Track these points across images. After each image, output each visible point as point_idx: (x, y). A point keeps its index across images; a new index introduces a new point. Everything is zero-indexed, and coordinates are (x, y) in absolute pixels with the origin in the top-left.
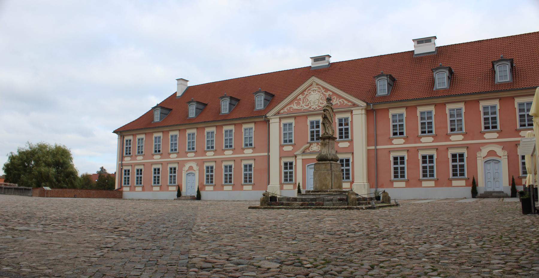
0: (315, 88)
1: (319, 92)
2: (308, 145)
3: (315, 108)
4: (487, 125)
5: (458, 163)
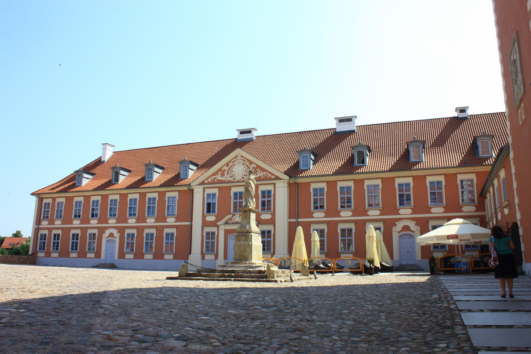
0: (240, 159)
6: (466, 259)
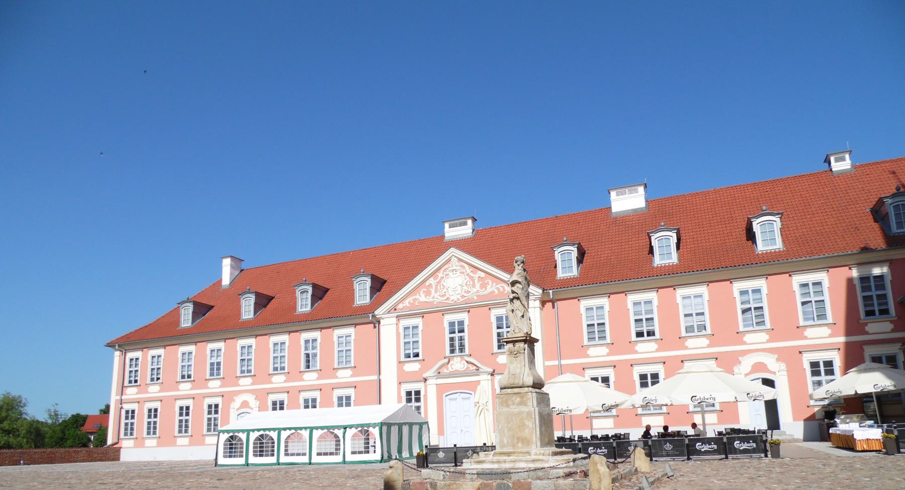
0: (456, 266)
2: (446, 360)
4: (869, 308)
6: (392, 428)
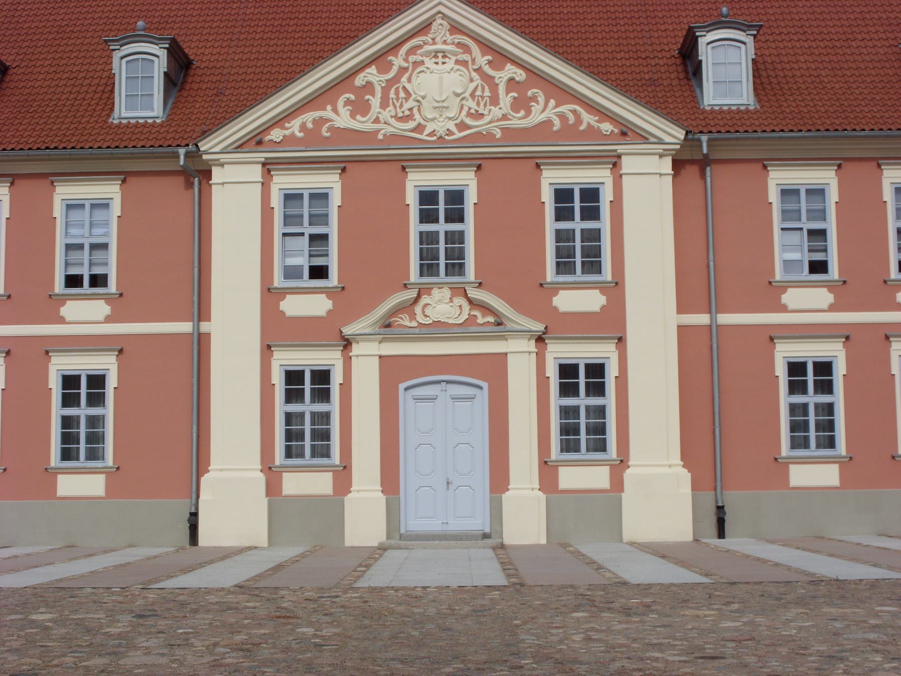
0: (445, 42)
1: (464, 63)
3: (441, 132)
5: (812, 399)
